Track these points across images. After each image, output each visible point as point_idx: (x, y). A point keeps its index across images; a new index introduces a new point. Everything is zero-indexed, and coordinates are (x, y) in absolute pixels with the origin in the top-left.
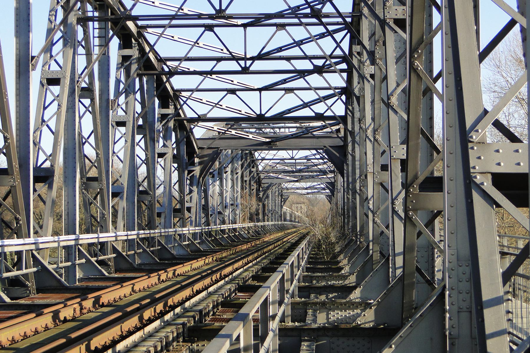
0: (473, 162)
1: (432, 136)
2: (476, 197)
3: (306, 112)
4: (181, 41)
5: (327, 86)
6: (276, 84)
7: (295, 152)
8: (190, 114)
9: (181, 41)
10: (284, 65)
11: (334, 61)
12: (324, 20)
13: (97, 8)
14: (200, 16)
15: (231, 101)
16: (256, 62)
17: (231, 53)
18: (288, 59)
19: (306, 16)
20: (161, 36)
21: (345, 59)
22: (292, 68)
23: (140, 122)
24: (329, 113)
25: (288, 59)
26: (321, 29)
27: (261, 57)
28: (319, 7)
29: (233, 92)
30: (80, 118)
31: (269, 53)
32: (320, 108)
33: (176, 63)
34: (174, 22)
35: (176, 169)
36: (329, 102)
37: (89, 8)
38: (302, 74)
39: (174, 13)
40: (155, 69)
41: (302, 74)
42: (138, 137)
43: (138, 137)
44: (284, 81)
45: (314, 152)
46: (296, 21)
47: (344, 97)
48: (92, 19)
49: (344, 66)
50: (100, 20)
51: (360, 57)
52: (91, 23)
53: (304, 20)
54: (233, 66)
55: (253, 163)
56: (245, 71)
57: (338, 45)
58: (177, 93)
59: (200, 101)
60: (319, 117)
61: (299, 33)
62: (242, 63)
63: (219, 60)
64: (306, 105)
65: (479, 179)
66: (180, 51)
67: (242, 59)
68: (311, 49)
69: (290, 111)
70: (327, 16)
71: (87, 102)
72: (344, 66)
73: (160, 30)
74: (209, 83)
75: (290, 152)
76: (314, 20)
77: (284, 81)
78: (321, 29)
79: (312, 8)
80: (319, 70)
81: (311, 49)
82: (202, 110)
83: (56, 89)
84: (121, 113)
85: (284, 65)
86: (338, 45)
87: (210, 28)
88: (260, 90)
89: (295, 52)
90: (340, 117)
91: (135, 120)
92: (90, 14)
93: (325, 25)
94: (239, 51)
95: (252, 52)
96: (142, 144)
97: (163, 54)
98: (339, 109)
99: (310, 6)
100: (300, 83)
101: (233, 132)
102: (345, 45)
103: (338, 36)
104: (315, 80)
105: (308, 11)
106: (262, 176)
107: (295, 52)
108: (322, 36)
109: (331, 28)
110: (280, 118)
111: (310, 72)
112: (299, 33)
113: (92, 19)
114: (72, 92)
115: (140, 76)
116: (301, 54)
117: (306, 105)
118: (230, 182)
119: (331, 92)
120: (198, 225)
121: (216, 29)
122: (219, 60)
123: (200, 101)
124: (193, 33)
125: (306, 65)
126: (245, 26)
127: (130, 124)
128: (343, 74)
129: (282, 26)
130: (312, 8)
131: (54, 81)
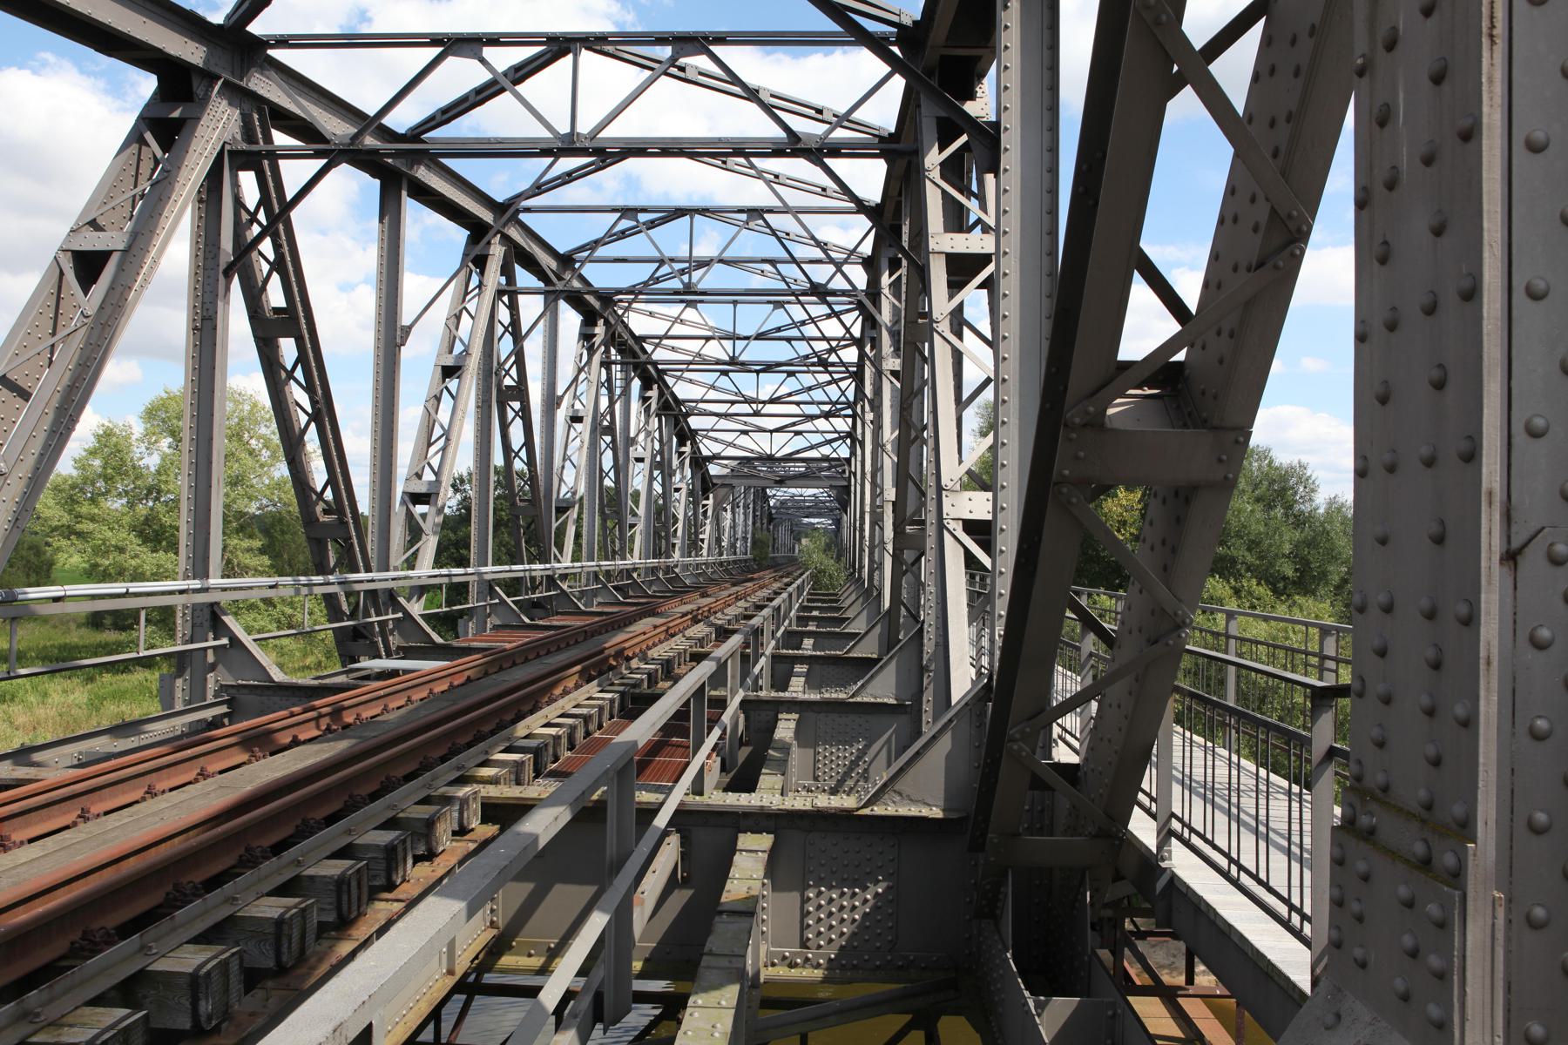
0: (946, 508)
1: (921, 481)
2: (947, 536)
3: (814, 454)
4: (663, 317)
5: (832, 429)
6: (786, 426)
7: (804, 490)
8: (705, 452)
9: (663, 317)
10: (793, 409)
11: (839, 406)
12: (830, 369)
13: (1093, 928)
14: (718, 362)
15: (744, 441)
16: (767, 406)
17: (743, 396)
18: (798, 404)
19: (813, 364)
20: (657, 345)
21: (849, 405)
22: (801, 412)
23: (658, 459)
24: (834, 455)
25: (798, 404)
26: (827, 377)
27: (772, 401)
28: (826, 356)
29: (745, 432)
30: (601, 454)
31: (779, 398)
32: (826, 450)
33: (694, 404)
34: (691, 367)
35: (517, 414)
36: (835, 445)
37: (613, 351)
38: (811, 418)
39: (691, 358)
40: (674, 410)
41: (811, 418)
42: (656, 473)
43: (656, 473)
44: (794, 424)
45: (821, 490)
46: (805, 368)
47: (848, 441)
48: (615, 363)
49: (849, 412)
50: (622, 363)
51: (726, 661)
52: (613, 366)
53: (812, 368)
54: (745, 408)
55: (766, 498)
56: (756, 414)
57: (843, 393)
58: (694, 433)
59: (716, 440)
60: (826, 459)
61: (808, 380)
62: (754, 406)
63: (733, 403)
64: (812, 447)
65: (952, 525)
66: (658, 327)
67: (754, 402)
68: (818, 395)
69: (798, 452)
70: (833, 365)
71: (608, 439)
72: (849, 412)
73: (679, 374)
74: (724, 424)
75: (799, 490)
76: (821, 369)
77: (794, 424)
78: (827, 377)
79: (819, 357)
80: (827, 415)
81: (818, 395)
82: (716, 448)
83: (578, 426)
84: (640, 449)
85: (793, 409)
86: (843, 393)
87: (725, 373)
88: (771, 432)
89: (804, 397)
90: (845, 459)
91: (653, 457)
92: (613, 358)
93: (830, 373)
94: (751, 393)
95: (764, 396)
96: (659, 479)
97: (680, 396)
98: (844, 452)
99: (817, 356)
100: (808, 426)
101: (746, 470)
102: (851, 394)
103: (843, 385)
104: (822, 424)
105: (815, 360)
106: (773, 511)
107: (804, 397)
108: (829, 383)
109: (836, 376)
110: (788, 458)
111: (817, 417)
112: (808, 380)
113: (615, 363)
114: (593, 430)
115: (659, 416)
116: (809, 399)
117: (812, 447)
118: (742, 516)
119: (836, 435)
120: (362, 594)
121: (730, 374)
122: (733, 403)
123: (716, 440)
124: (709, 378)
125: (813, 410)
126: (758, 372)
127: (648, 461)
128: (847, 419)
129: (791, 374)
130: (819, 357)
131: (576, 419)
